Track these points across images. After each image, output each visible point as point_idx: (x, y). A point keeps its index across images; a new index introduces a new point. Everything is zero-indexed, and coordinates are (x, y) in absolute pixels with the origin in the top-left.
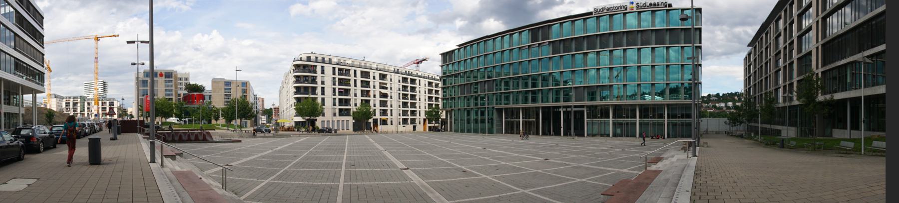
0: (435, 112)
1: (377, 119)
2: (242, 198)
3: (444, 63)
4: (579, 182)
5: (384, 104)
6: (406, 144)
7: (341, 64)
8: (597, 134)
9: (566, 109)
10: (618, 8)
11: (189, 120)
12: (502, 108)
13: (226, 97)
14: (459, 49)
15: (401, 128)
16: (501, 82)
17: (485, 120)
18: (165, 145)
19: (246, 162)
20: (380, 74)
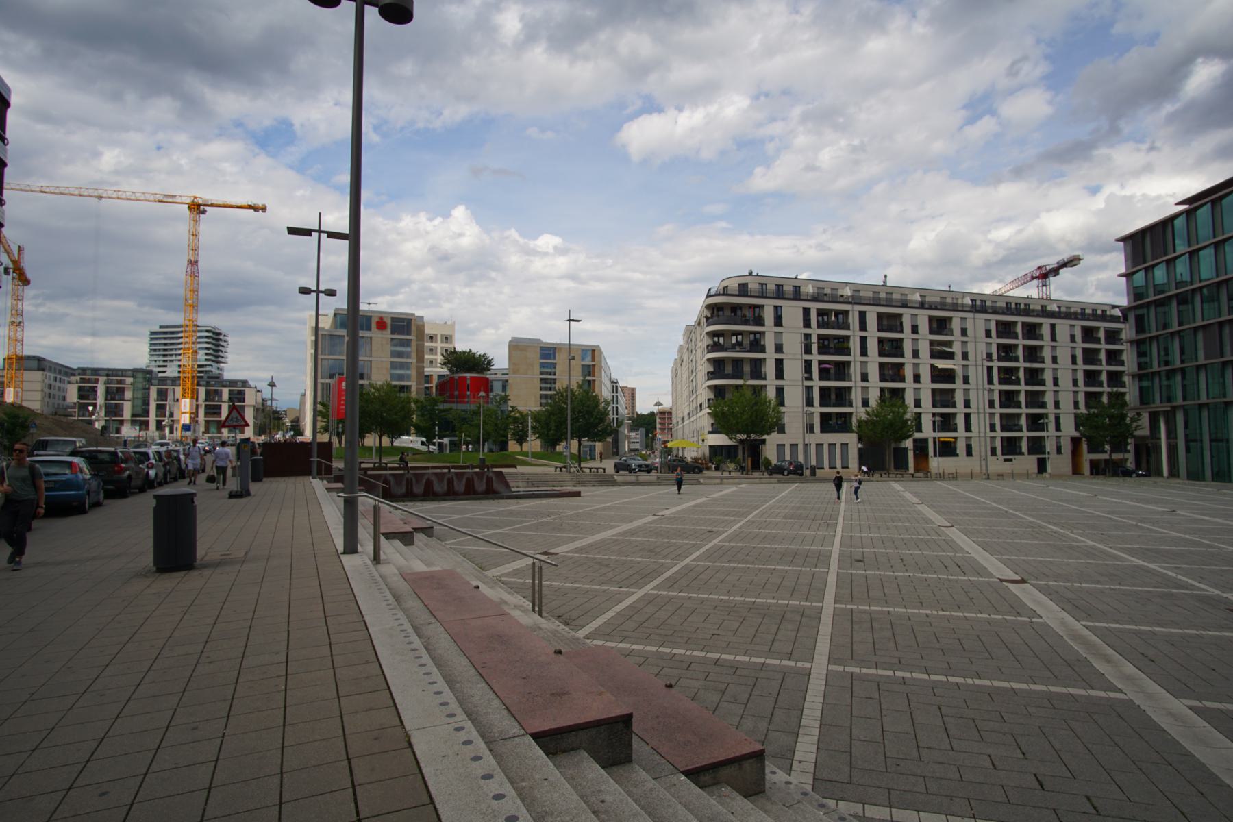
0: (1111, 417)
1: (925, 441)
2: (581, 633)
3: (1134, 265)
7: (825, 298)
11: (451, 442)
13: (544, 385)
18: (385, 507)
19: (591, 545)
20: (931, 319)
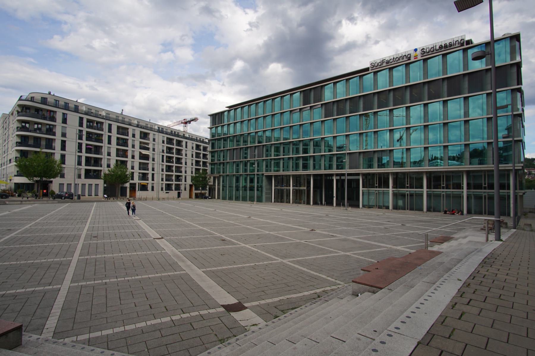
0: (202, 178)
1: (135, 184)
3: (213, 125)
4: (342, 256)
5: (144, 167)
6: (166, 212)
7: (92, 114)
8: (374, 206)
9: (340, 178)
10: (399, 59)
12: (272, 176)
14: (229, 111)
15: (163, 194)
16: (271, 147)
17: (254, 187)
20: (141, 132)
